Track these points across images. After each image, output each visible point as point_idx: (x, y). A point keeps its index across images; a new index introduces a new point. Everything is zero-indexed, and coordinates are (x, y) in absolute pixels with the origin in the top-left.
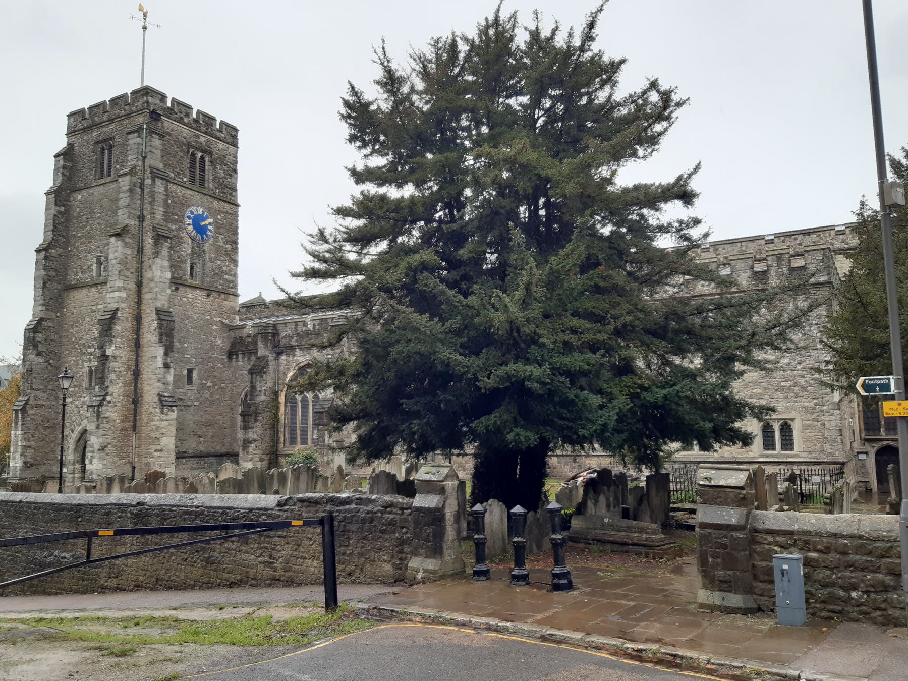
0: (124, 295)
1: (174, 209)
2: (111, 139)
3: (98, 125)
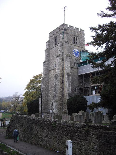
0: (59, 70)
1: (70, 50)
2: (57, 37)
3: (55, 34)
